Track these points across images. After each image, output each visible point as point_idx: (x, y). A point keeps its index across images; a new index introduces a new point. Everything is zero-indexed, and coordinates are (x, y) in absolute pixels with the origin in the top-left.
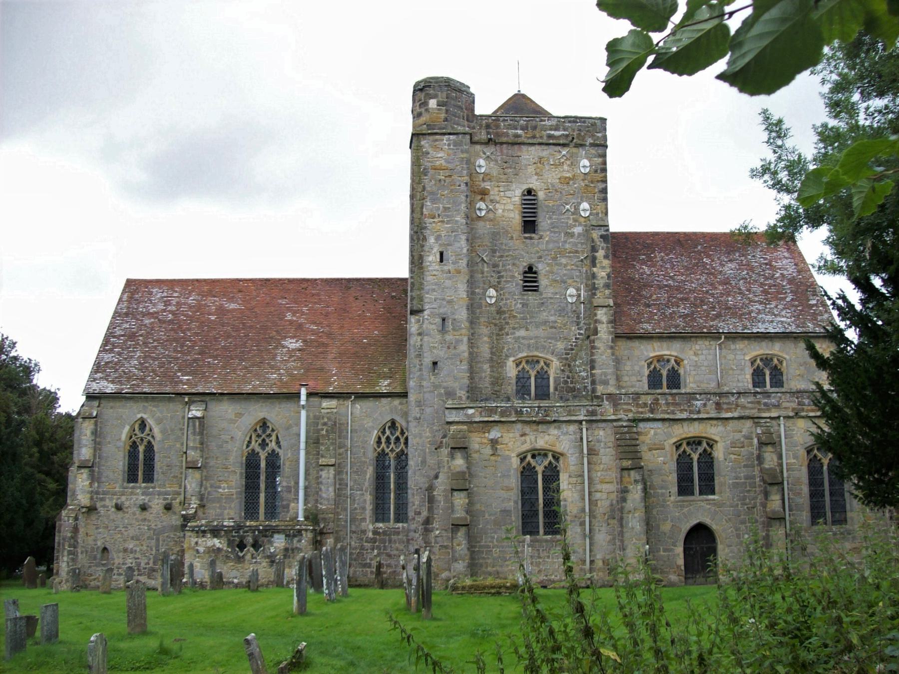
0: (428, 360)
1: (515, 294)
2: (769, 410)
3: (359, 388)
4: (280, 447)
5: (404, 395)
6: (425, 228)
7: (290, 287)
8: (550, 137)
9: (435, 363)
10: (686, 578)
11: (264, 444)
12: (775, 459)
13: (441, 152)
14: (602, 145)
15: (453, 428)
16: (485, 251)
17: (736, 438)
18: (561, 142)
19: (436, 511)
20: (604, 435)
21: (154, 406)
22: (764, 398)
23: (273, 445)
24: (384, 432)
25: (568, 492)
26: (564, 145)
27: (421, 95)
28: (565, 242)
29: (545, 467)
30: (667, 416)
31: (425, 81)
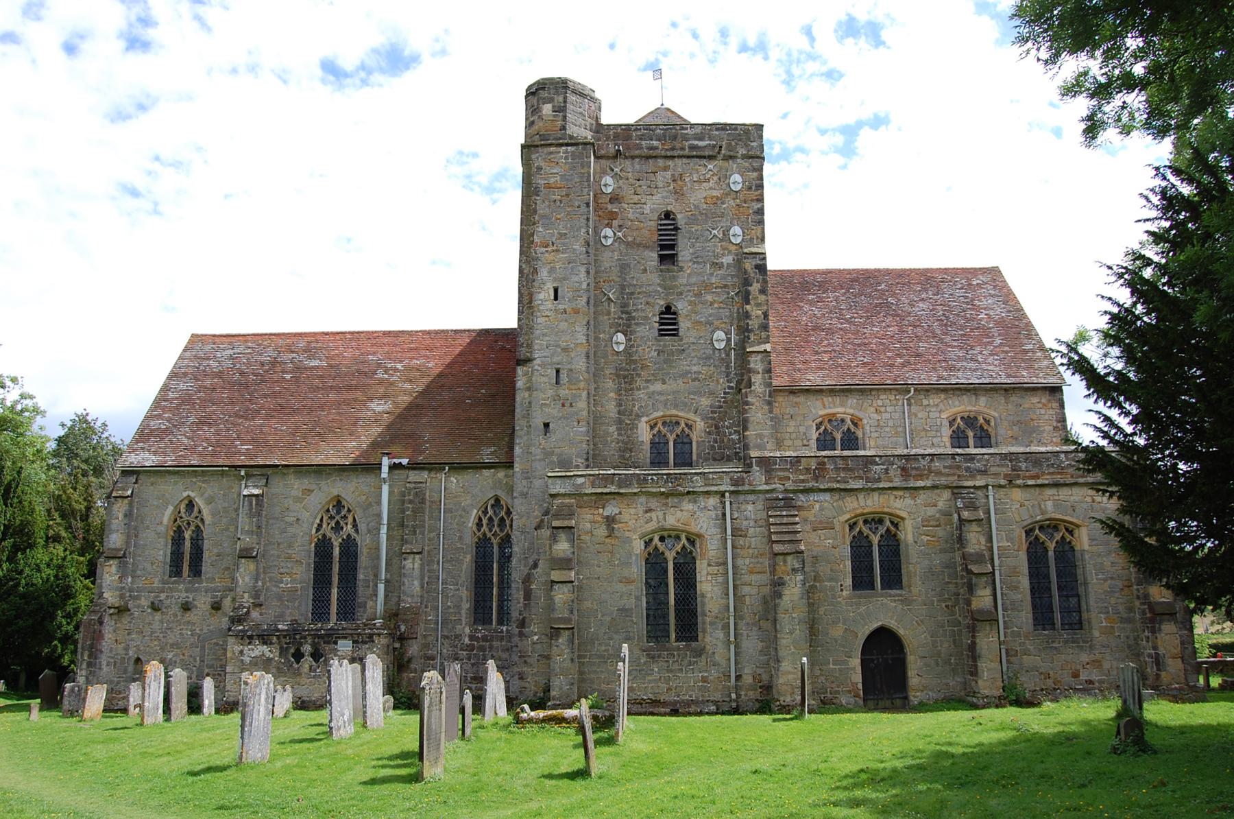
0: (538, 421)
1: (648, 340)
2: (973, 477)
3: (455, 458)
4: (357, 531)
5: (509, 465)
6: (537, 259)
7: (386, 340)
8: (693, 148)
9: (546, 425)
10: (865, 700)
11: (338, 528)
12: (983, 540)
13: (556, 167)
14: (756, 158)
15: (558, 501)
16: (611, 288)
17: (929, 514)
18: (707, 153)
19: (534, 611)
20: (751, 510)
21: (204, 482)
22: (967, 461)
23: (349, 529)
24: (485, 512)
25: (708, 585)
26: (711, 158)
27: (534, 100)
28: (712, 274)
29: (678, 553)
30: (836, 486)
31: (538, 83)
